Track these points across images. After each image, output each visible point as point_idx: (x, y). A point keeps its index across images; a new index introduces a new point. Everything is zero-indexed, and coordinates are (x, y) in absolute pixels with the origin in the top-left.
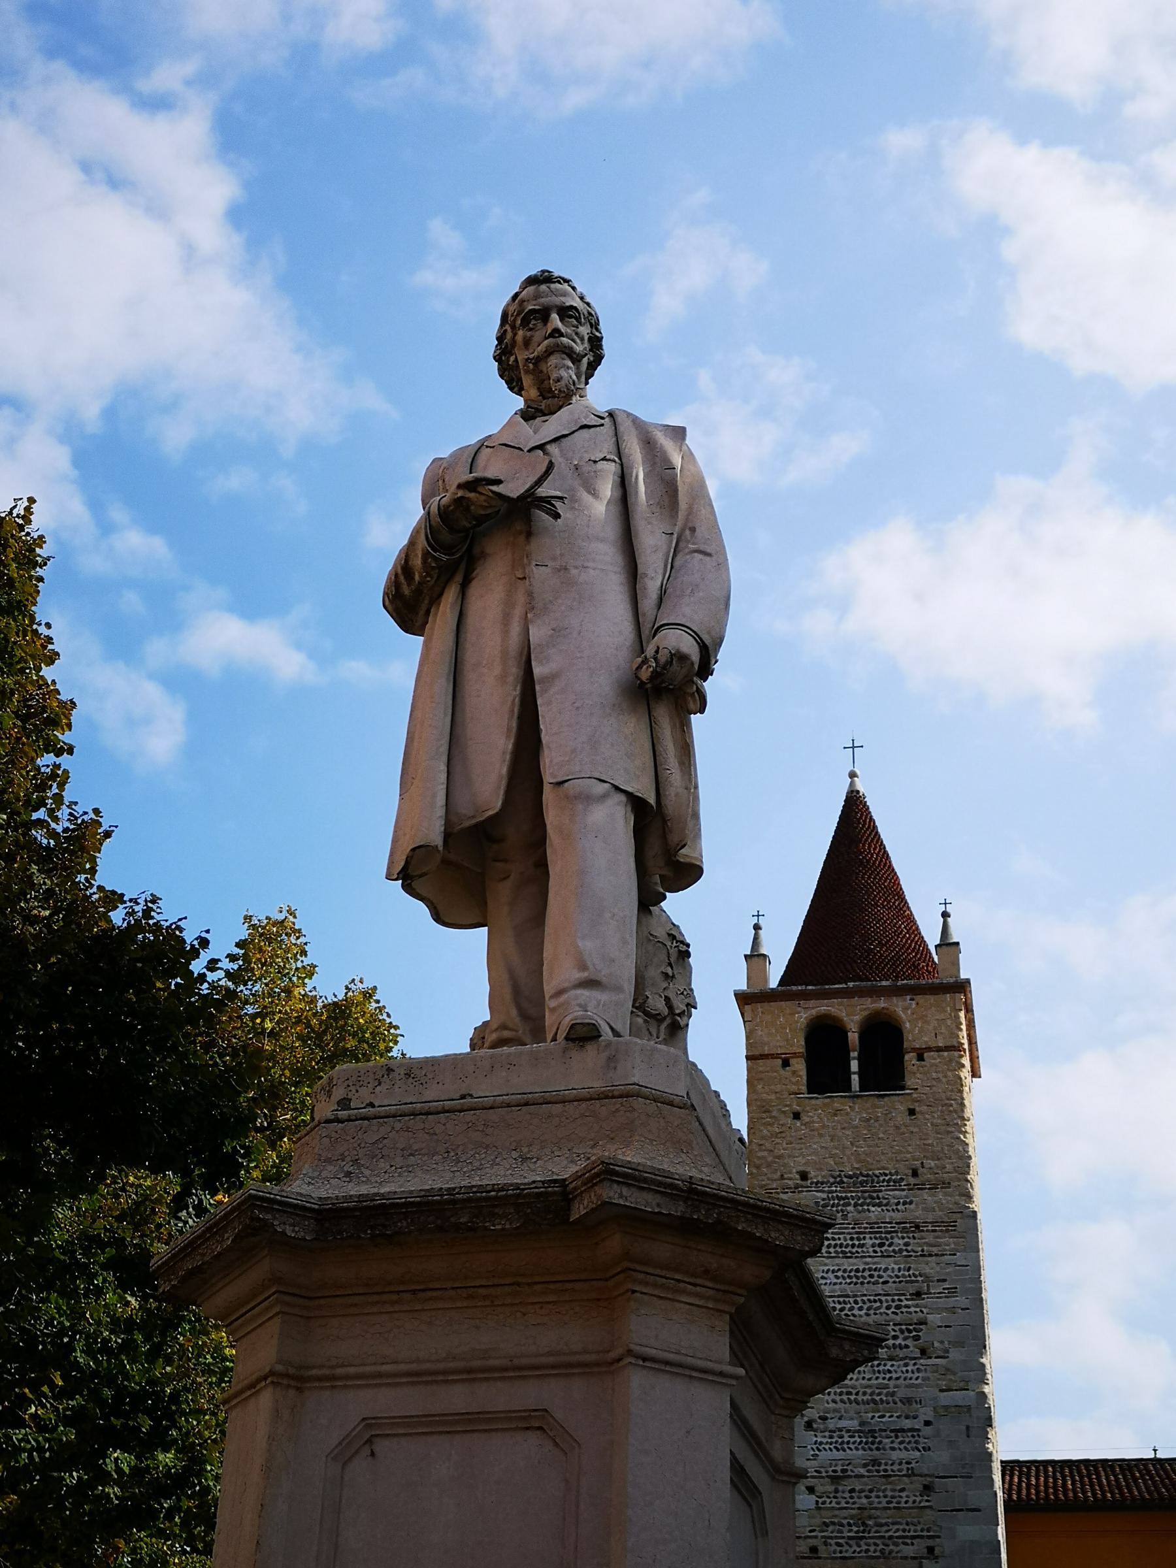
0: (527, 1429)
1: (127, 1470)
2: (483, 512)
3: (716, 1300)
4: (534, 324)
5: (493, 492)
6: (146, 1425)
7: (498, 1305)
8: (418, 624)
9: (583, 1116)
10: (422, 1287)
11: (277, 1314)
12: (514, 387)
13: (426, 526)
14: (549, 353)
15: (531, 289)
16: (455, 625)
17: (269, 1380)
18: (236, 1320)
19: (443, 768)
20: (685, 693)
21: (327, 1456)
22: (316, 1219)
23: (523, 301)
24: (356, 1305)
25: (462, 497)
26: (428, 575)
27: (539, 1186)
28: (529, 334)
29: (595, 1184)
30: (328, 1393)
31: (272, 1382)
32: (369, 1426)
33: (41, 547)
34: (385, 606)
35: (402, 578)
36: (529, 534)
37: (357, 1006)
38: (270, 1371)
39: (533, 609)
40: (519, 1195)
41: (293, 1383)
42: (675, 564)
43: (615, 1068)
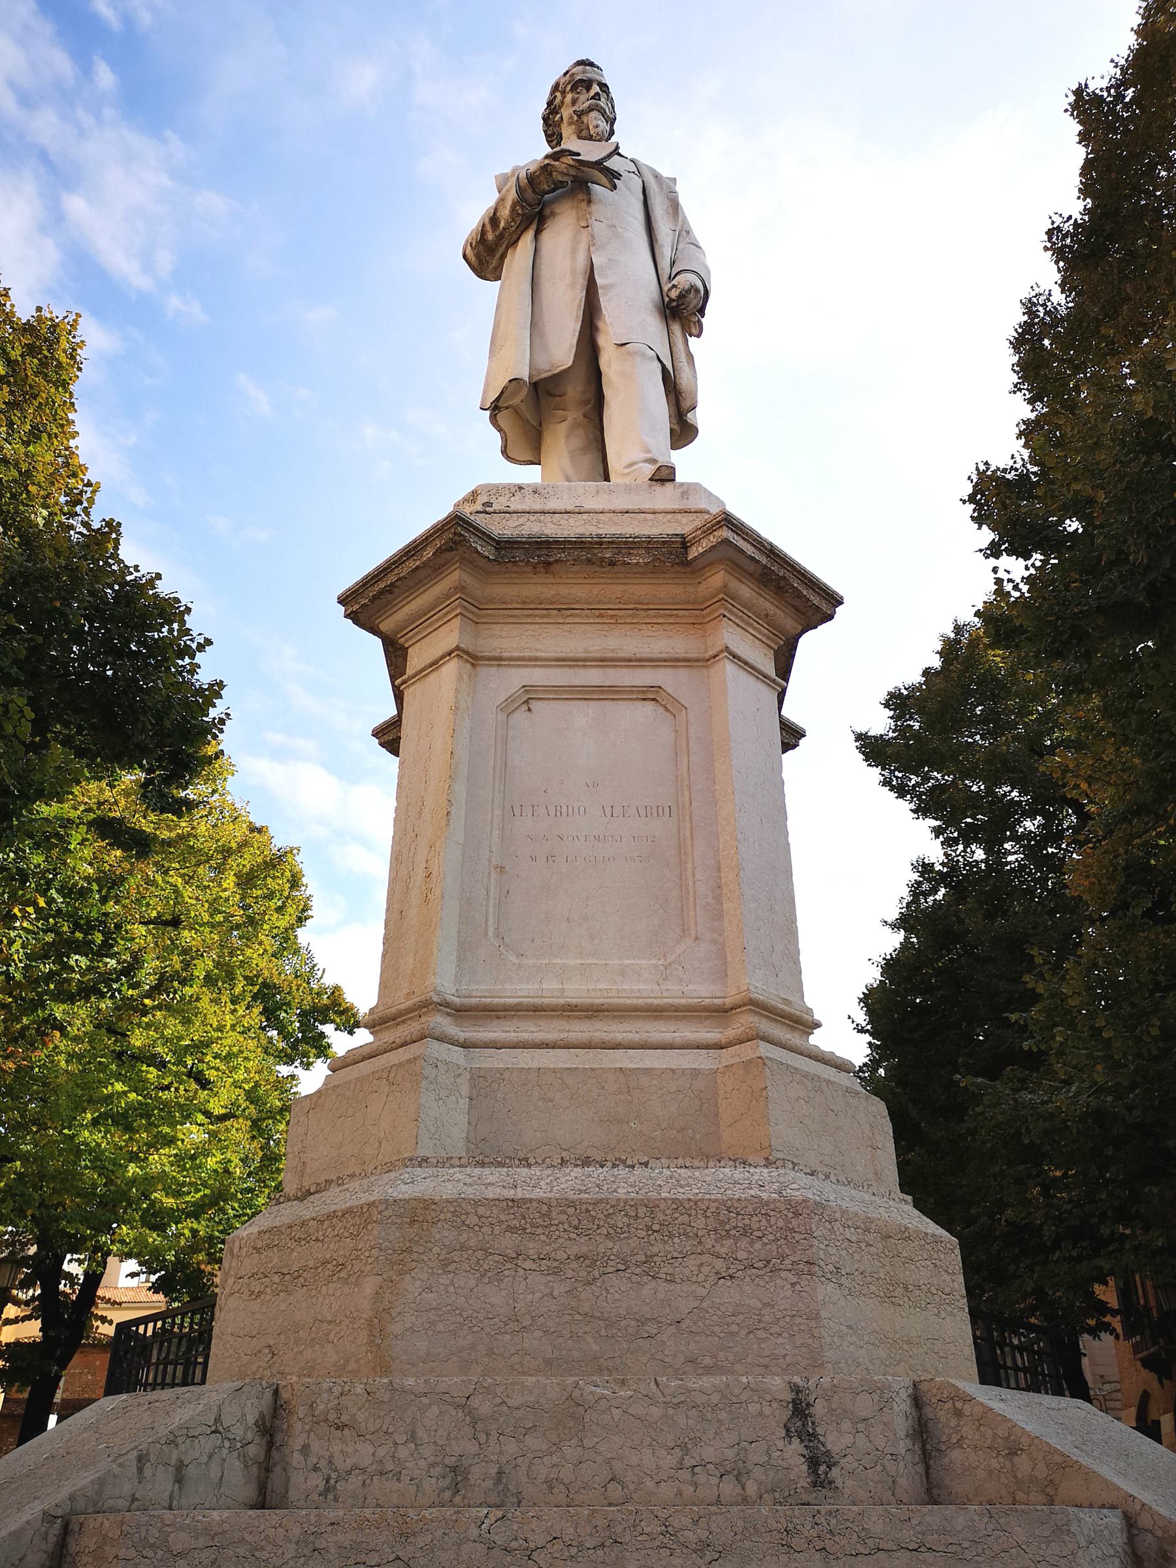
0: (644, 699)
1: (84, 967)
2: (560, 179)
3: (768, 638)
5: (573, 159)
6: (99, 938)
9: (669, 521)
10: (565, 607)
11: (457, 615)
12: (552, 141)
14: (591, 109)
15: (580, 68)
17: (455, 654)
23: (573, 74)
24: (515, 616)
25: (548, 164)
26: (513, 220)
28: (576, 96)
29: (715, 530)
30: (495, 669)
33: (82, 348)
34: (465, 256)
35: (488, 227)
36: (589, 202)
41: (470, 660)
42: (679, 247)
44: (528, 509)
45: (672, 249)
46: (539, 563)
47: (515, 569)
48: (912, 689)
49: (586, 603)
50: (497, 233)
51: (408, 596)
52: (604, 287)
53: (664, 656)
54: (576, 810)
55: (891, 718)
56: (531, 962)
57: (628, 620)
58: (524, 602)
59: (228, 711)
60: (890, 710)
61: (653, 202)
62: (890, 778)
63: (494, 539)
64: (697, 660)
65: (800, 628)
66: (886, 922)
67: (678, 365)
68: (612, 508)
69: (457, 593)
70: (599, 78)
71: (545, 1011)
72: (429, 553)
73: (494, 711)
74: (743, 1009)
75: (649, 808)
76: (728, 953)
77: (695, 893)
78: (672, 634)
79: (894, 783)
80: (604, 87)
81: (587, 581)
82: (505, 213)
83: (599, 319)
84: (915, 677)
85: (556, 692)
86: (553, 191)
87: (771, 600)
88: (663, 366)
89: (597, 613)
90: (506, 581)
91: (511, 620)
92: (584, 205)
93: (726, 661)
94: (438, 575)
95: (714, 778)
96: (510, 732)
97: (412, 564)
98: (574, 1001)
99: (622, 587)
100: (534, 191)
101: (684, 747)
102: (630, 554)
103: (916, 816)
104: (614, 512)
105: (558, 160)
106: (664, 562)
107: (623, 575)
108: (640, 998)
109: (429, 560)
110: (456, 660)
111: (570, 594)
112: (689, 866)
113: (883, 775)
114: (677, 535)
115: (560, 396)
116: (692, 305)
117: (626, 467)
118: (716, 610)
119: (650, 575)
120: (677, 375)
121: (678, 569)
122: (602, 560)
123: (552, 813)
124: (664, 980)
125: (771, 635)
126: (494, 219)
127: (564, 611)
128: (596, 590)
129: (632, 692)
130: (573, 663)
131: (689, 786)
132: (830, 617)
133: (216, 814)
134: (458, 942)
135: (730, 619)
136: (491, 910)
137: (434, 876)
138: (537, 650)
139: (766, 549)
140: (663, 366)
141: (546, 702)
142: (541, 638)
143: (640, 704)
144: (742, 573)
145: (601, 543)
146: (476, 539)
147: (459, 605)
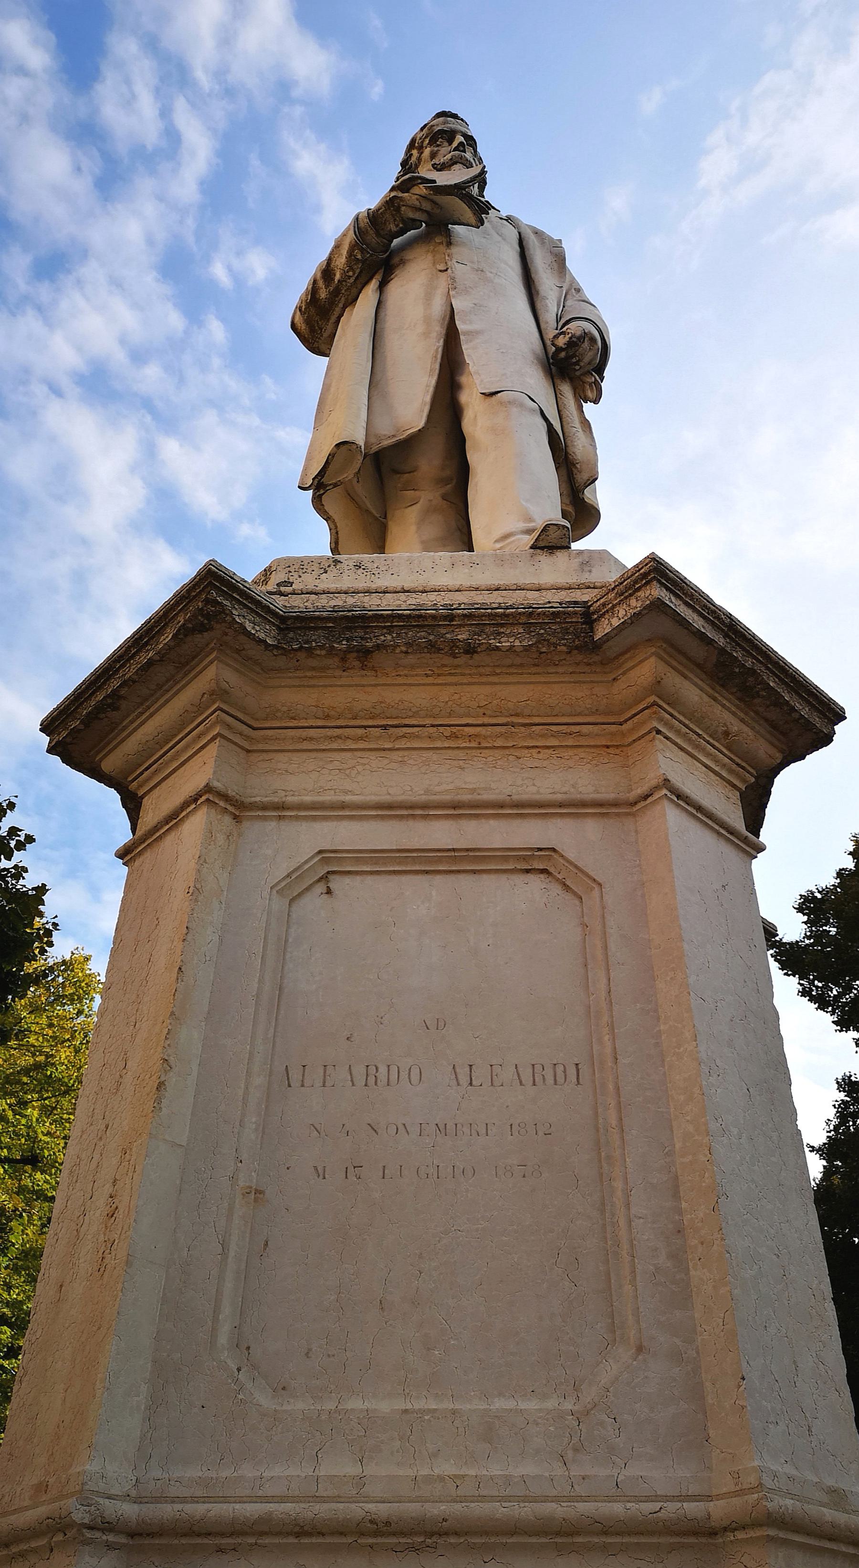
0: (528, 871)
3: (731, 771)
4: (441, 142)
7: (486, 748)
8: (325, 335)
10: (395, 722)
11: (213, 739)
13: (354, 227)
16: (374, 311)
18: (147, 769)
19: (366, 393)
20: (584, 382)
21: (271, 888)
22: (278, 628)
24: (311, 739)
25: (394, 197)
26: (351, 268)
27: (555, 606)
28: (436, 149)
30: (273, 824)
31: (208, 800)
32: (325, 861)
34: (293, 327)
35: (321, 284)
37: (78, 964)
38: (207, 785)
39: (455, 288)
40: (531, 614)
43: (590, 571)
44: (344, 588)
45: (558, 306)
46: (349, 650)
47: (314, 663)
48: (825, 892)
49: (426, 716)
50: (332, 289)
51: (142, 713)
52: (467, 333)
53: (559, 797)
54: (404, 1075)
55: (805, 923)
56: (300, 1405)
57: (499, 743)
58: (327, 717)
59: (55, 920)
60: (804, 914)
61: (532, 252)
62: (810, 988)
63: (274, 614)
64: (615, 804)
65: (779, 757)
66: (813, 1147)
67: (570, 431)
68: (474, 584)
69: (214, 702)
70: (463, 129)
71: (322, 1534)
72: (167, 637)
73: (266, 894)
74: (752, 1534)
75: (538, 1068)
76: (708, 1384)
77: (632, 1246)
78: (570, 763)
79: (814, 993)
80: (471, 141)
81: (430, 680)
82: (341, 261)
83: (461, 374)
84: (829, 880)
85: (376, 861)
86: (402, 232)
87: (733, 709)
88: (550, 426)
89: (447, 731)
90: (297, 682)
91: (306, 745)
92: (442, 248)
93: (666, 803)
94: (186, 675)
95: (656, 1011)
96: (292, 930)
97: (143, 658)
98: (382, 1510)
99: (487, 690)
100: (378, 234)
101: (599, 953)
102: (499, 634)
103: (839, 1028)
104: (477, 589)
105: (408, 192)
106: (555, 645)
107: (488, 670)
108: (526, 1499)
109: (169, 648)
110: (204, 810)
111: (402, 701)
112: (619, 1185)
113: (801, 985)
114: (576, 603)
115: (409, 472)
116: (587, 359)
117: (497, 541)
118: (644, 723)
119: (534, 670)
120: (569, 443)
121: (580, 658)
122: (454, 643)
123: (360, 1080)
124: (576, 1450)
125: (734, 766)
126: (327, 272)
127: (392, 730)
128: (445, 694)
129: (506, 859)
130: (405, 812)
131: (612, 1027)
132: (827, 739)
133: (79, 1037)
134: (155, 1362)
135: (667, 738)
136: (229, 1285)
137: (119, 1215)
138: (346, 792)
139: (723, 623)
140: (550, 426)
141: (358, 878)
142: (354, 772)
143: (519, 879)
144: (685, 661)
145: (451, 618)
146: (244, 612)
147: (218, 721)
